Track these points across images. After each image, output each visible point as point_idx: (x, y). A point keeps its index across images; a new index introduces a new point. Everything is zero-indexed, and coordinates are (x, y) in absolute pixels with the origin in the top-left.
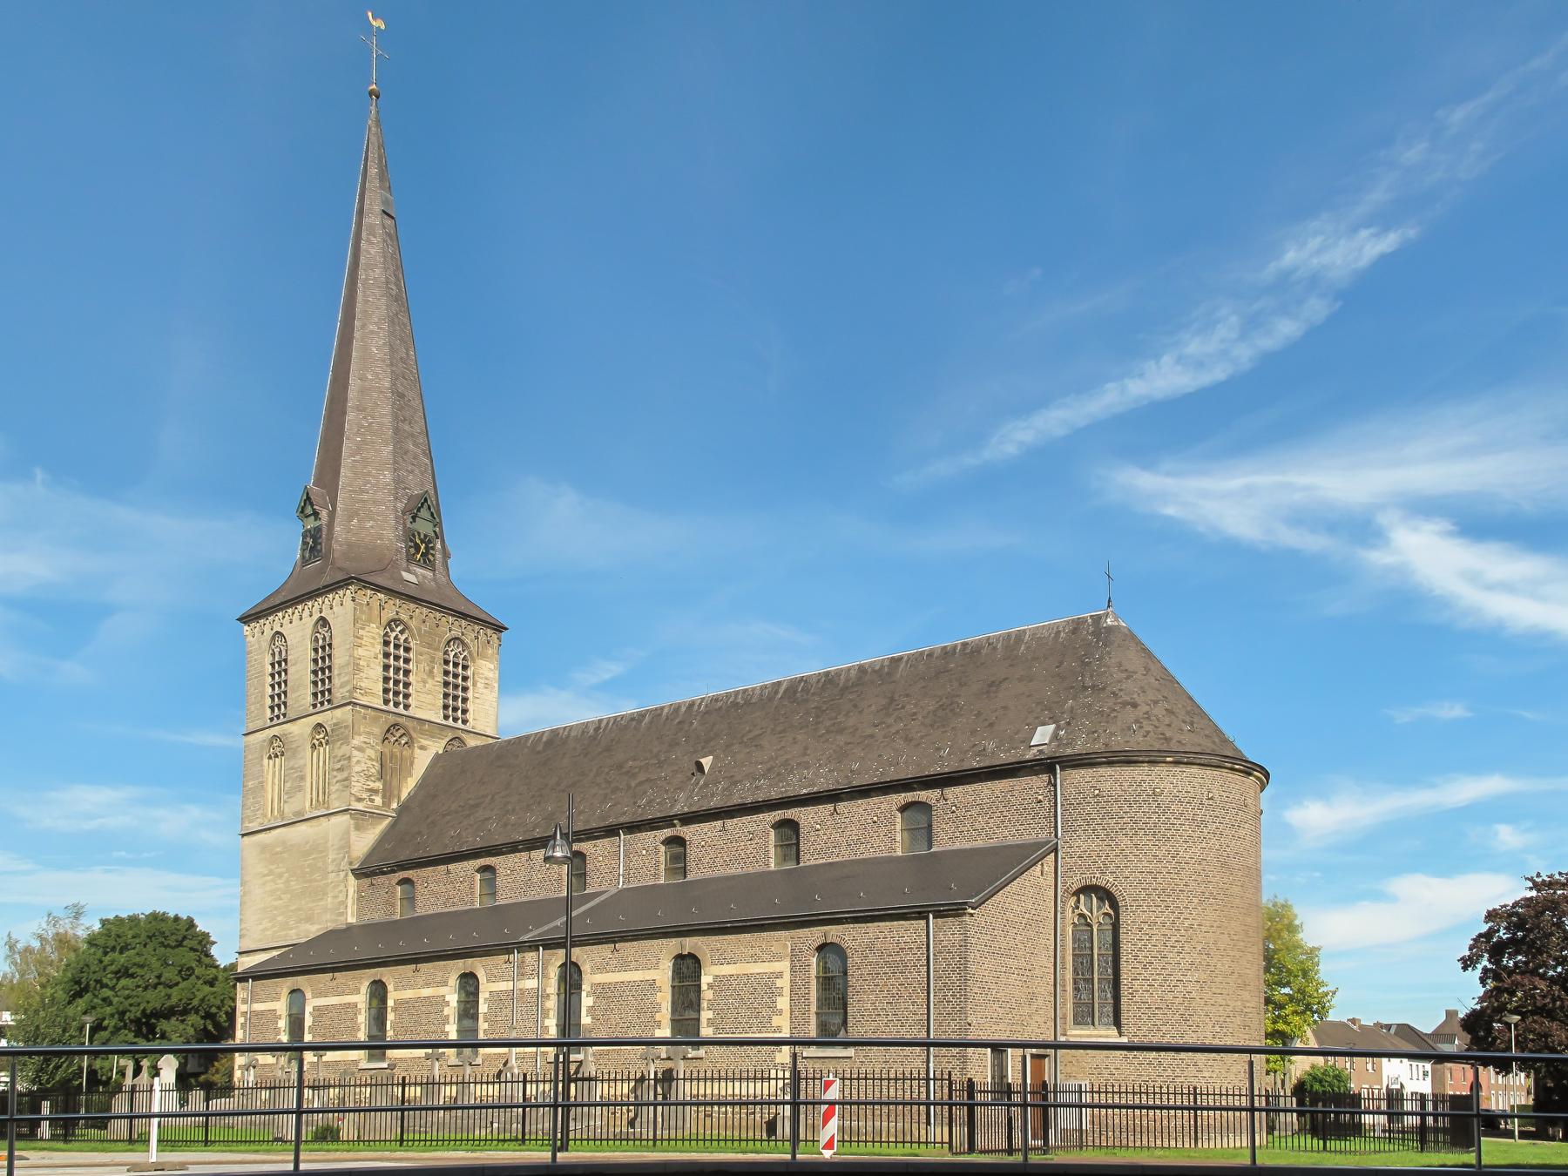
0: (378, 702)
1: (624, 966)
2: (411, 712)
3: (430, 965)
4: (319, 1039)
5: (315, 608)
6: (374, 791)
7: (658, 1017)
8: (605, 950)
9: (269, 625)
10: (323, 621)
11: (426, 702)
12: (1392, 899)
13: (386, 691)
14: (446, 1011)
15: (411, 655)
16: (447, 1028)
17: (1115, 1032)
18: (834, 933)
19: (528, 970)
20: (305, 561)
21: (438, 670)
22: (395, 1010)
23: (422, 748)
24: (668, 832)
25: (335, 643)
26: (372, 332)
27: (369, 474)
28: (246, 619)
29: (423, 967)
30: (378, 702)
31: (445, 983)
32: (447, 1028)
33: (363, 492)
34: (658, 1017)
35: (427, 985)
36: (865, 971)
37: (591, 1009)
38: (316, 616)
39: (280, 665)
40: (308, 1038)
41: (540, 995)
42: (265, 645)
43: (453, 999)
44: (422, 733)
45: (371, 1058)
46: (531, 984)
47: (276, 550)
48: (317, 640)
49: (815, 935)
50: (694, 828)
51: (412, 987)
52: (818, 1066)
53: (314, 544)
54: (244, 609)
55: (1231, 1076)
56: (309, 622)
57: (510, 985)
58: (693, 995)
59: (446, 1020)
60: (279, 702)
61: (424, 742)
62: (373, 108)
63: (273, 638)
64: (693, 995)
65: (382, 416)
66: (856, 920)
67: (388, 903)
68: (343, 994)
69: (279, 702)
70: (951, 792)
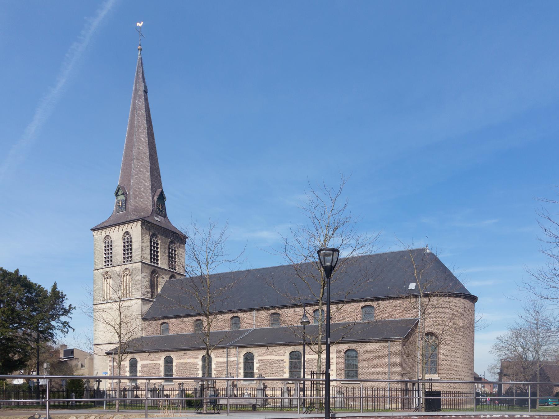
0: (148, 262)
1: (272, 354)
2: (159, 265)
3: (191, 352)
4: (143, 375)
5: (125, 228)
6: (148, 292)
7: (285, 370)
8: (264, 349)
9: (104, 233)
10: (127, 233)
11: (163, 263)
12: (55, 287)
13: (151, 258)
14: (198, 367)
15: (159, 246)
16: (198, 372)
17: (437, 375)
18: (353, 346)
19: (232, 355)
20: (117, 211)
21: (167, 251)
22: (176, 366)
23: (163, 278)
24: (272, 311)
25: (133, 240)
26: (141, 132)
27: (142, 182)
28: (93, 230)
29: (188, 352)
30: (148, 262)
31: (197, 358)
32: (198, 372)
33: (139, 188)
34: (285, 370)
35: (190, 358)
36: (365, 358)
37: (258, 368)
38: (125, 231)
39: (109, 247)
40: (139, 374)
41: (238, 363)
42: (102, 240)
43: (200, 363)
44: (162, 273)
45: (165, 382)
46: (234, 359)
47: (109, 206)
48: (124, 239)
49: (346, 346)
50: (283, 310)
51: (184, 359)
52: (346, 386)
53: (123, 206)
54: (93, 227)
55: (468, 388)
56: (121, 233)
57: (225, 359)
58: (298, 364)
59: (198, 370)
60: (109, 260)
61: (163, 276)
62: (139, 54)
63: (105, 237)
64: (298, 364)
65: (146, 162)
66: (361, 342)
67: (153, 330)
68: (154, 360)
69: (109, 260)
70: (381, 303)
